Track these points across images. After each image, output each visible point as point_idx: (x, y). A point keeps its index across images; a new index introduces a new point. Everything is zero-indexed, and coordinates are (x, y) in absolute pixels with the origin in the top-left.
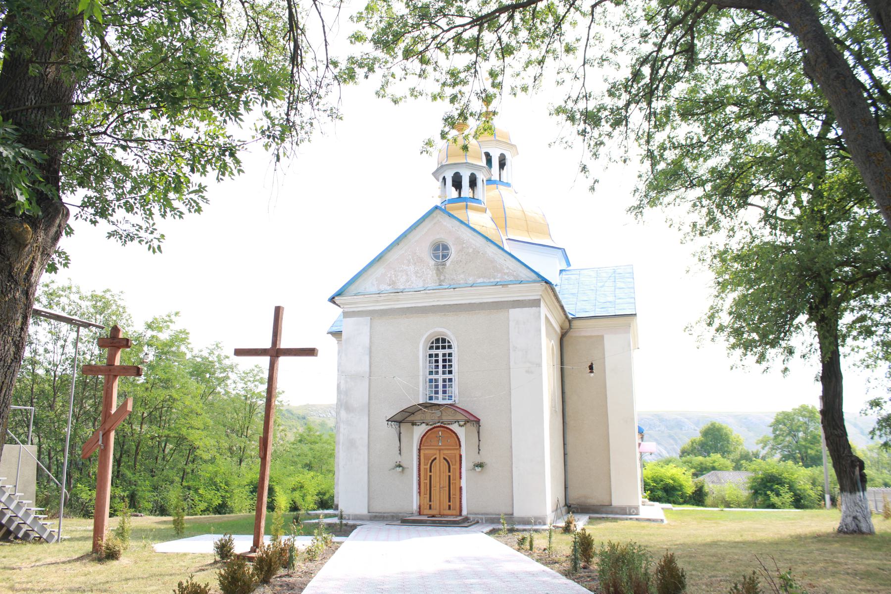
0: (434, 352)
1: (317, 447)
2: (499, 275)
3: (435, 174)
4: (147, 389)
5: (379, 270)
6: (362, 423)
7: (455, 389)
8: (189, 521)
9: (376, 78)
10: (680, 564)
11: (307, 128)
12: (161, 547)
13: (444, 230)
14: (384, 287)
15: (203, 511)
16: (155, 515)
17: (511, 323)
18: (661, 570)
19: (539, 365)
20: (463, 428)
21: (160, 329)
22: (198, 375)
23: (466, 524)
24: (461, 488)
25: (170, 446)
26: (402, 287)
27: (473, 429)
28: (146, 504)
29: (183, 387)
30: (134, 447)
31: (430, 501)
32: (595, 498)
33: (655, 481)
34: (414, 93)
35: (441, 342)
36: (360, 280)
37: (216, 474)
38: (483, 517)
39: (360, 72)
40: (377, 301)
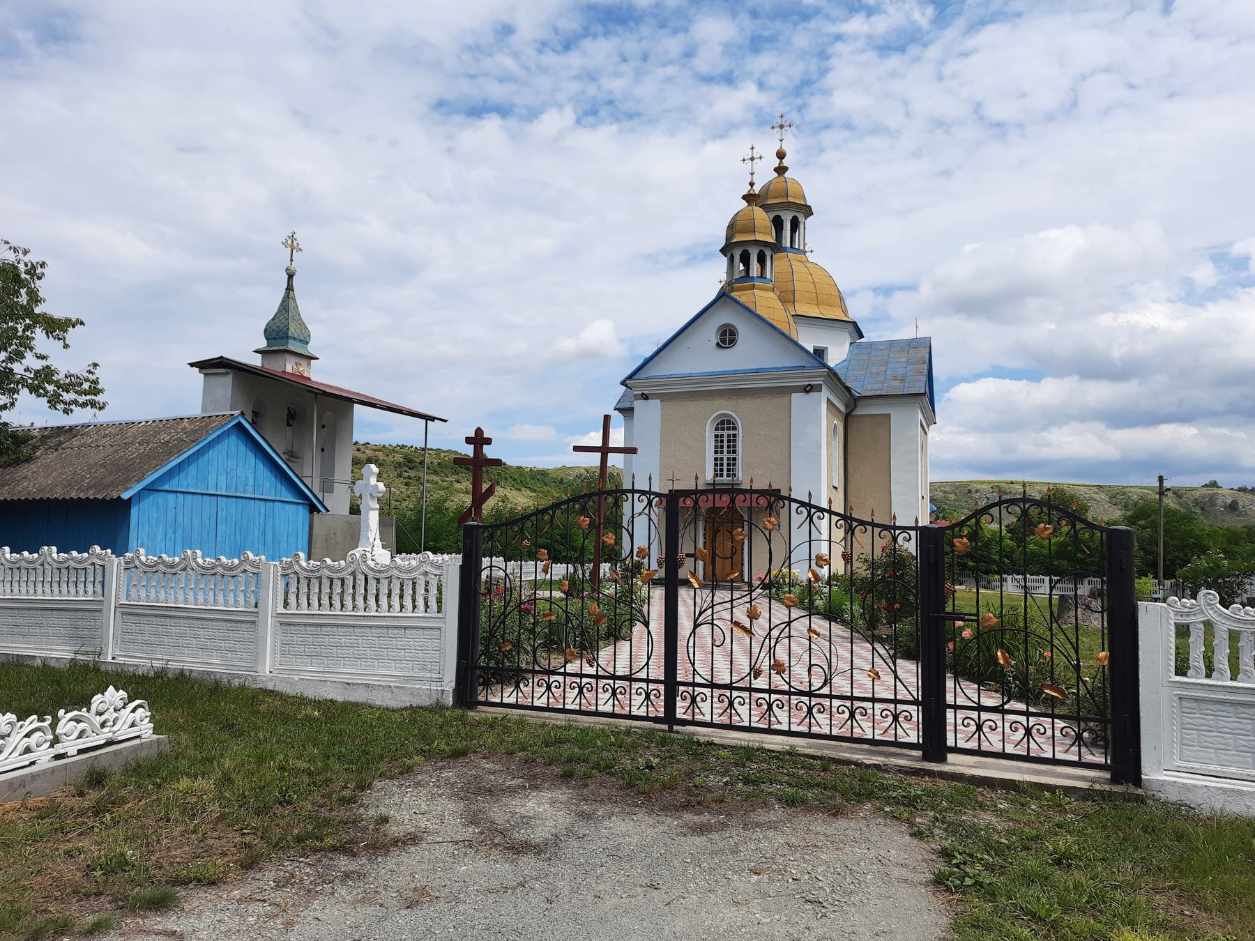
0: (719, 433)
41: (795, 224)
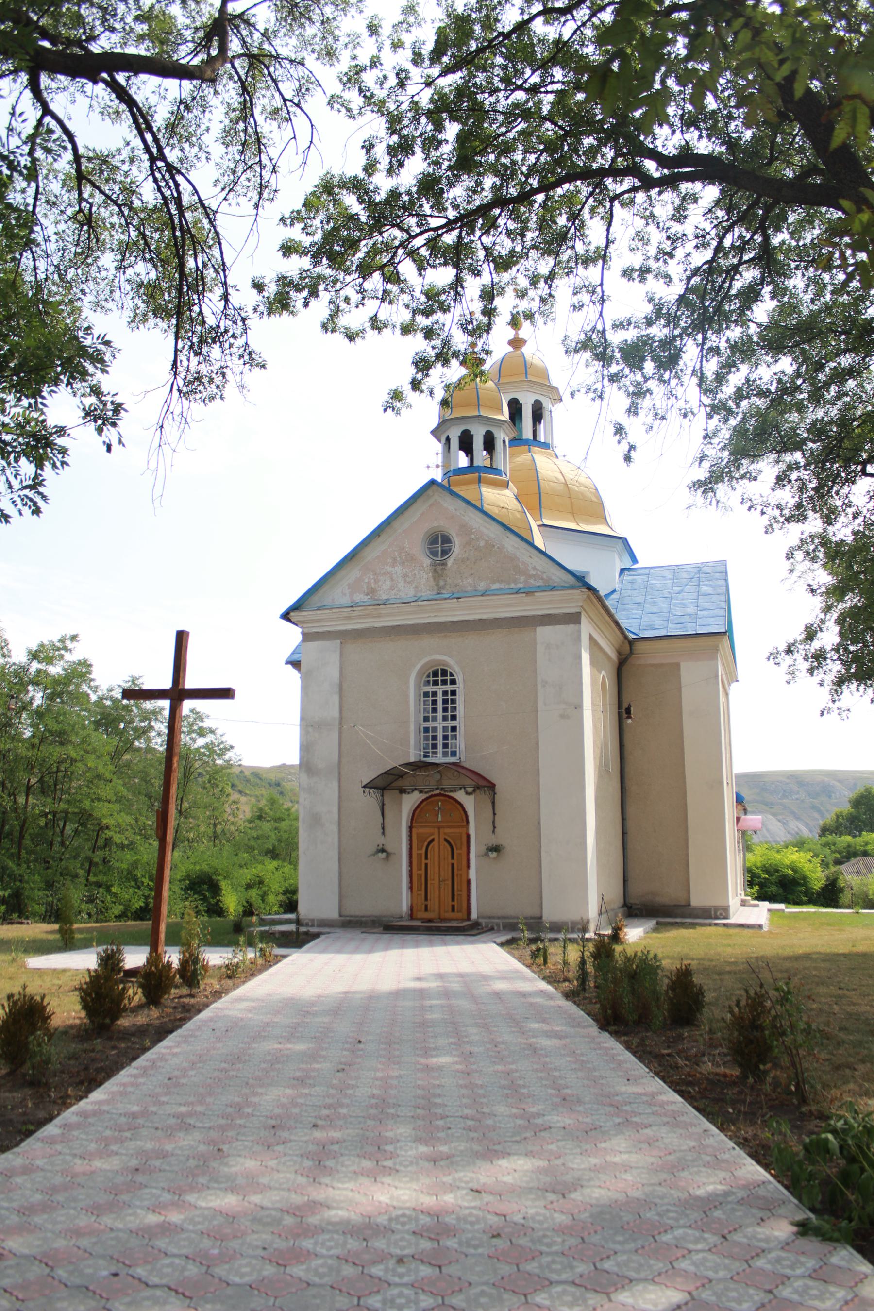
0: (431, 689)
1: (283, 825)
2: (522, 578)
3: (435, 433)
4: (33, 746)
5: (353, 573)
6: (330, 790)
7: (460, 742)
8: (80, 931)
9: (320, 307)
10: (696, 979)
11: (218, 380)
12: (36, 962)
13: (447, 514)
14: (360, 597)
15: (118, 918)
16: (49, 923)
17: (538, 647)
18: (673, 986)
19: (579, 707)
20: (472, 797)
21: (50, 661)
22: (107, 726)
23: (475, 932)
24: (469, 882)
25: (69, 829)
26: (384, 597)
27: (486, 799)
28: (36, 907)
29: (83, 742)
30: (18, 828)
31: (426, 899)
32: (669, 894)
33: (766, 870)
34: (376, 324)
35: (440, 675)
36: (326, 588)
37: (135, 865)
38: (500, 921)
39: (297, 298)
40: (349, 618)
41: (538, 415)
